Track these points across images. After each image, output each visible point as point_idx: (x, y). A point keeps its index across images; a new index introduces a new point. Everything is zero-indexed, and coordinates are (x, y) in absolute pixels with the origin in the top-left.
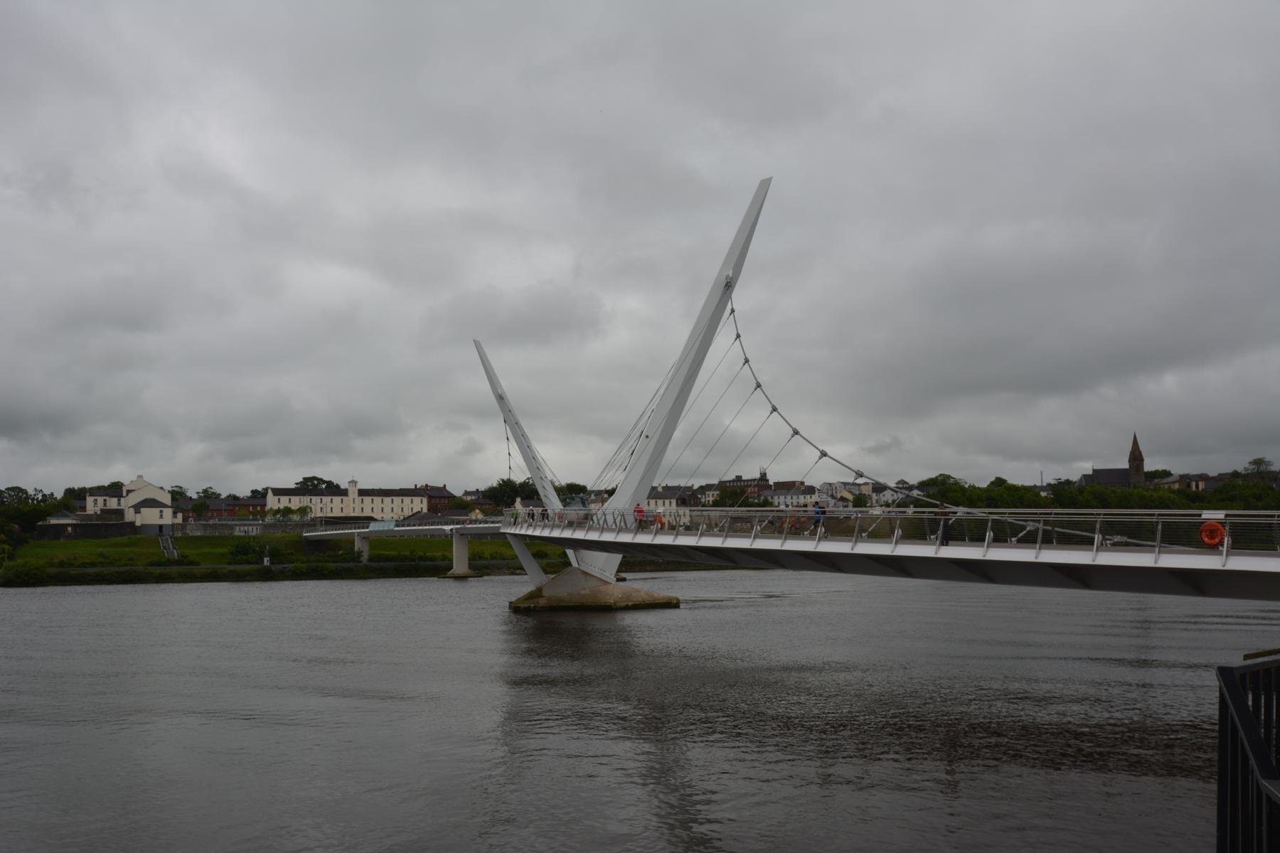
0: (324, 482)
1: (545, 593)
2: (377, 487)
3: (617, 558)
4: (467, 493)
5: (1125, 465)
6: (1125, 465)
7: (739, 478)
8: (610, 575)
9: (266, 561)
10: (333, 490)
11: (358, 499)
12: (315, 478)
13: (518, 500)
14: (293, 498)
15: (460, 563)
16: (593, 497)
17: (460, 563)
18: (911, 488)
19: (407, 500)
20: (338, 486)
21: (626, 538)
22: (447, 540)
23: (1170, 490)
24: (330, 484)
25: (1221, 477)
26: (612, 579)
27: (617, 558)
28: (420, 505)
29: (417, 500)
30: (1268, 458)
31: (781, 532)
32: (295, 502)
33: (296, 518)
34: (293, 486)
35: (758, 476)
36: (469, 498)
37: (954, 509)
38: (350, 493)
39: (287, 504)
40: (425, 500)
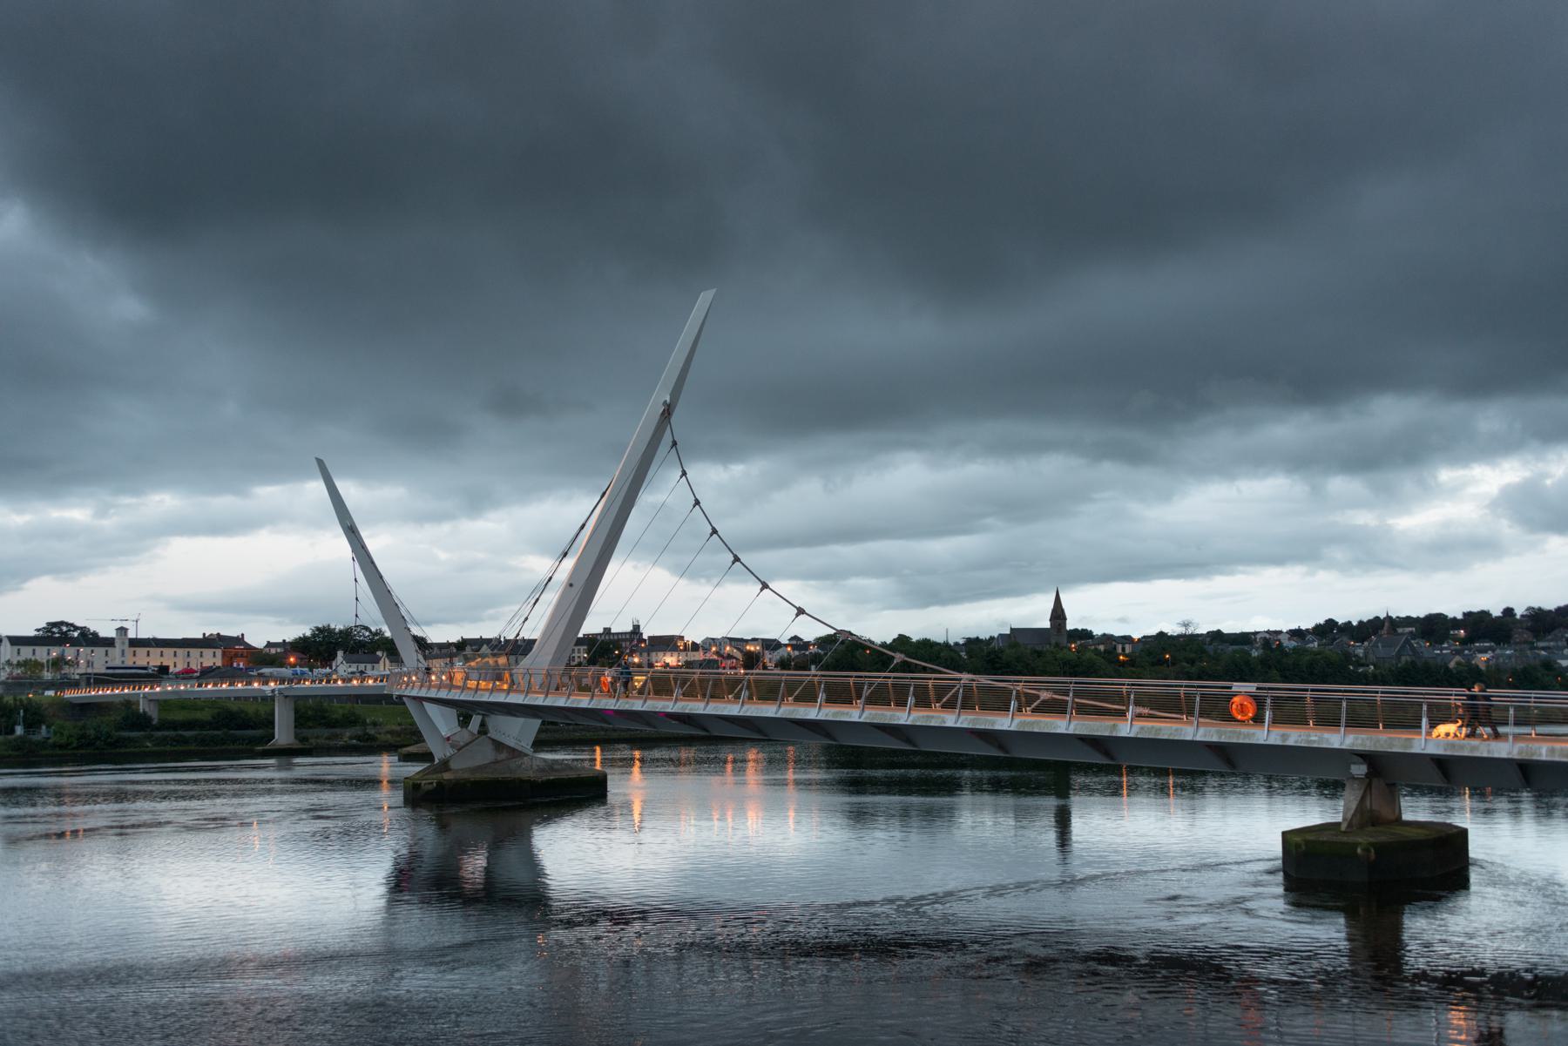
0: (76, 628)
1: (453, 765)
2: (180, 636)
3: (536, 724)
4: (270, 645)
5: (1046, 624)
6: (1046, 624)
7: (607, 631)
8: (526, 745)
9: (19, 730)
10: (89, 639)
11: (129, 651)
12: (62, 623)
13: (340, 654)
14: (38, 649)
15: (283, 734)
16: (436, 650)
17: (283, 734)
18: (807, 644)
19: (195, 652)
20: (95, 634)
21: (539, 700)
22: (268, 700)
23: (1097, 652)
24: (84, 632)
25: (1145, 640)
26: (528, 749)
27: (536, 724)
28: (212, 658)
29: (208, 652)
30: (1196, 621)
31: (1190, 713)
32: (42, 654)
33: (47, 675)
34: (32, 633)
35: (629, 628)
36: (273, 651)
37: (958, 675)
38: (117, 644)
39: (30, 656)
40: (219, 652)
